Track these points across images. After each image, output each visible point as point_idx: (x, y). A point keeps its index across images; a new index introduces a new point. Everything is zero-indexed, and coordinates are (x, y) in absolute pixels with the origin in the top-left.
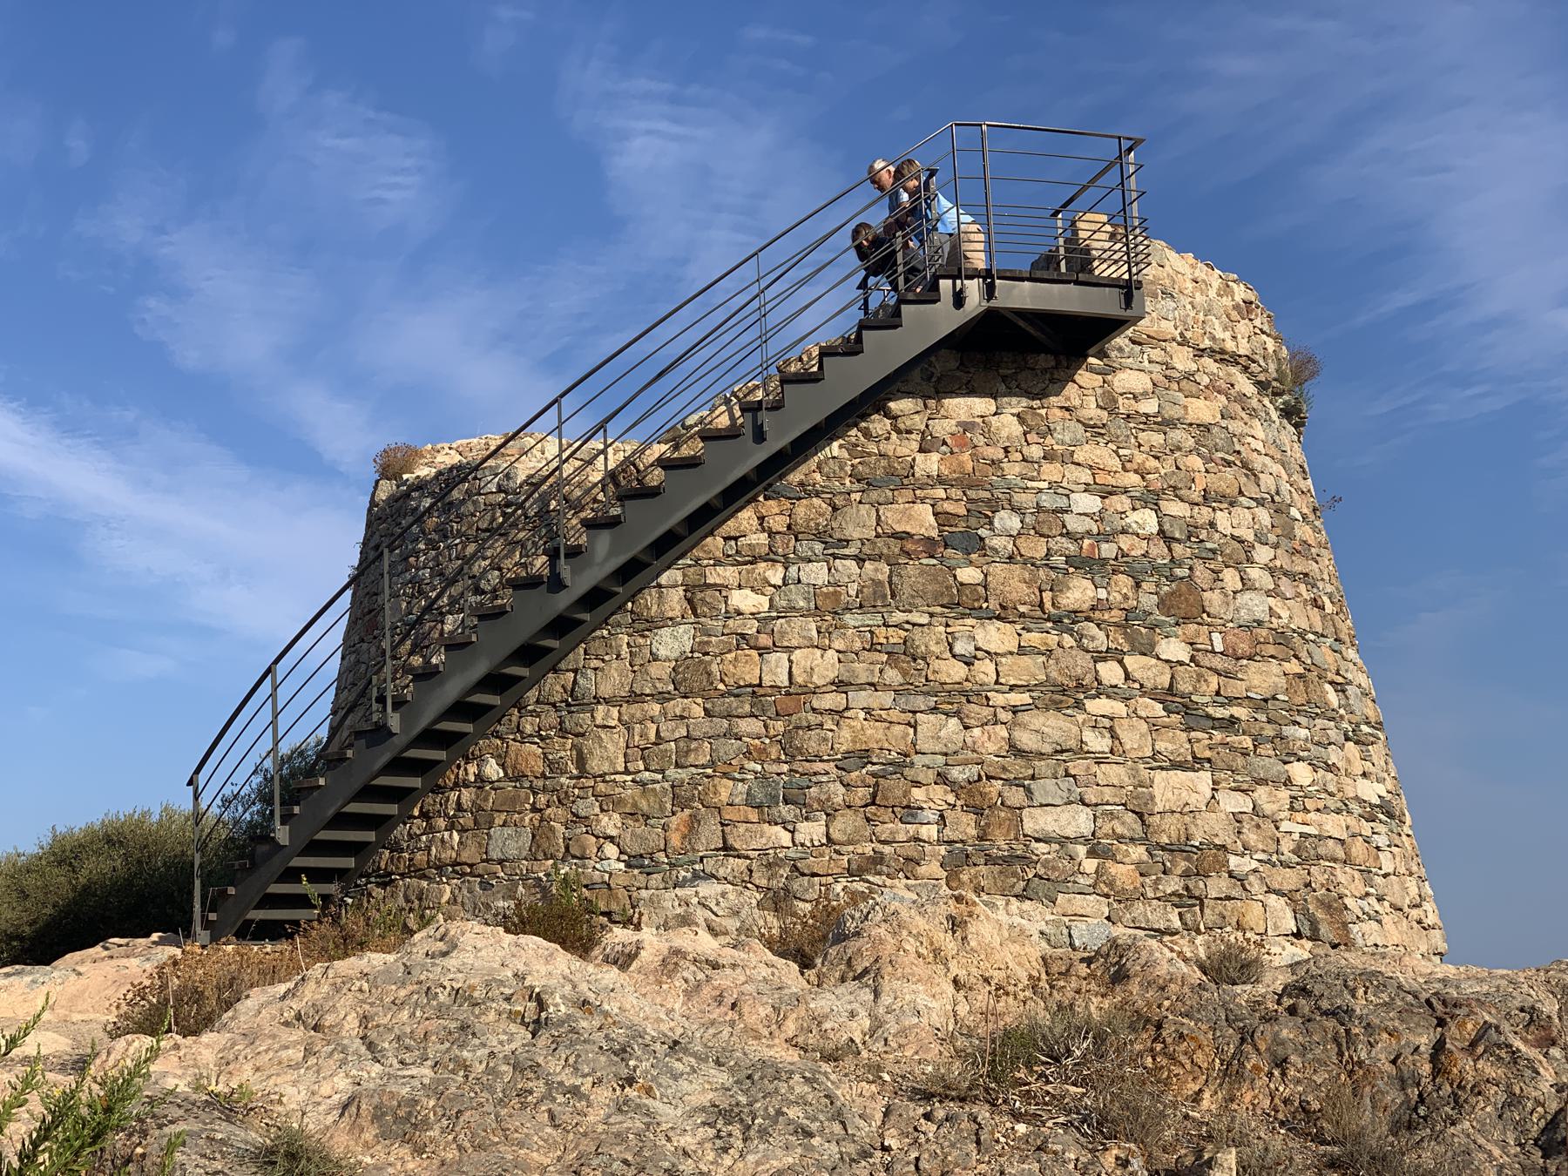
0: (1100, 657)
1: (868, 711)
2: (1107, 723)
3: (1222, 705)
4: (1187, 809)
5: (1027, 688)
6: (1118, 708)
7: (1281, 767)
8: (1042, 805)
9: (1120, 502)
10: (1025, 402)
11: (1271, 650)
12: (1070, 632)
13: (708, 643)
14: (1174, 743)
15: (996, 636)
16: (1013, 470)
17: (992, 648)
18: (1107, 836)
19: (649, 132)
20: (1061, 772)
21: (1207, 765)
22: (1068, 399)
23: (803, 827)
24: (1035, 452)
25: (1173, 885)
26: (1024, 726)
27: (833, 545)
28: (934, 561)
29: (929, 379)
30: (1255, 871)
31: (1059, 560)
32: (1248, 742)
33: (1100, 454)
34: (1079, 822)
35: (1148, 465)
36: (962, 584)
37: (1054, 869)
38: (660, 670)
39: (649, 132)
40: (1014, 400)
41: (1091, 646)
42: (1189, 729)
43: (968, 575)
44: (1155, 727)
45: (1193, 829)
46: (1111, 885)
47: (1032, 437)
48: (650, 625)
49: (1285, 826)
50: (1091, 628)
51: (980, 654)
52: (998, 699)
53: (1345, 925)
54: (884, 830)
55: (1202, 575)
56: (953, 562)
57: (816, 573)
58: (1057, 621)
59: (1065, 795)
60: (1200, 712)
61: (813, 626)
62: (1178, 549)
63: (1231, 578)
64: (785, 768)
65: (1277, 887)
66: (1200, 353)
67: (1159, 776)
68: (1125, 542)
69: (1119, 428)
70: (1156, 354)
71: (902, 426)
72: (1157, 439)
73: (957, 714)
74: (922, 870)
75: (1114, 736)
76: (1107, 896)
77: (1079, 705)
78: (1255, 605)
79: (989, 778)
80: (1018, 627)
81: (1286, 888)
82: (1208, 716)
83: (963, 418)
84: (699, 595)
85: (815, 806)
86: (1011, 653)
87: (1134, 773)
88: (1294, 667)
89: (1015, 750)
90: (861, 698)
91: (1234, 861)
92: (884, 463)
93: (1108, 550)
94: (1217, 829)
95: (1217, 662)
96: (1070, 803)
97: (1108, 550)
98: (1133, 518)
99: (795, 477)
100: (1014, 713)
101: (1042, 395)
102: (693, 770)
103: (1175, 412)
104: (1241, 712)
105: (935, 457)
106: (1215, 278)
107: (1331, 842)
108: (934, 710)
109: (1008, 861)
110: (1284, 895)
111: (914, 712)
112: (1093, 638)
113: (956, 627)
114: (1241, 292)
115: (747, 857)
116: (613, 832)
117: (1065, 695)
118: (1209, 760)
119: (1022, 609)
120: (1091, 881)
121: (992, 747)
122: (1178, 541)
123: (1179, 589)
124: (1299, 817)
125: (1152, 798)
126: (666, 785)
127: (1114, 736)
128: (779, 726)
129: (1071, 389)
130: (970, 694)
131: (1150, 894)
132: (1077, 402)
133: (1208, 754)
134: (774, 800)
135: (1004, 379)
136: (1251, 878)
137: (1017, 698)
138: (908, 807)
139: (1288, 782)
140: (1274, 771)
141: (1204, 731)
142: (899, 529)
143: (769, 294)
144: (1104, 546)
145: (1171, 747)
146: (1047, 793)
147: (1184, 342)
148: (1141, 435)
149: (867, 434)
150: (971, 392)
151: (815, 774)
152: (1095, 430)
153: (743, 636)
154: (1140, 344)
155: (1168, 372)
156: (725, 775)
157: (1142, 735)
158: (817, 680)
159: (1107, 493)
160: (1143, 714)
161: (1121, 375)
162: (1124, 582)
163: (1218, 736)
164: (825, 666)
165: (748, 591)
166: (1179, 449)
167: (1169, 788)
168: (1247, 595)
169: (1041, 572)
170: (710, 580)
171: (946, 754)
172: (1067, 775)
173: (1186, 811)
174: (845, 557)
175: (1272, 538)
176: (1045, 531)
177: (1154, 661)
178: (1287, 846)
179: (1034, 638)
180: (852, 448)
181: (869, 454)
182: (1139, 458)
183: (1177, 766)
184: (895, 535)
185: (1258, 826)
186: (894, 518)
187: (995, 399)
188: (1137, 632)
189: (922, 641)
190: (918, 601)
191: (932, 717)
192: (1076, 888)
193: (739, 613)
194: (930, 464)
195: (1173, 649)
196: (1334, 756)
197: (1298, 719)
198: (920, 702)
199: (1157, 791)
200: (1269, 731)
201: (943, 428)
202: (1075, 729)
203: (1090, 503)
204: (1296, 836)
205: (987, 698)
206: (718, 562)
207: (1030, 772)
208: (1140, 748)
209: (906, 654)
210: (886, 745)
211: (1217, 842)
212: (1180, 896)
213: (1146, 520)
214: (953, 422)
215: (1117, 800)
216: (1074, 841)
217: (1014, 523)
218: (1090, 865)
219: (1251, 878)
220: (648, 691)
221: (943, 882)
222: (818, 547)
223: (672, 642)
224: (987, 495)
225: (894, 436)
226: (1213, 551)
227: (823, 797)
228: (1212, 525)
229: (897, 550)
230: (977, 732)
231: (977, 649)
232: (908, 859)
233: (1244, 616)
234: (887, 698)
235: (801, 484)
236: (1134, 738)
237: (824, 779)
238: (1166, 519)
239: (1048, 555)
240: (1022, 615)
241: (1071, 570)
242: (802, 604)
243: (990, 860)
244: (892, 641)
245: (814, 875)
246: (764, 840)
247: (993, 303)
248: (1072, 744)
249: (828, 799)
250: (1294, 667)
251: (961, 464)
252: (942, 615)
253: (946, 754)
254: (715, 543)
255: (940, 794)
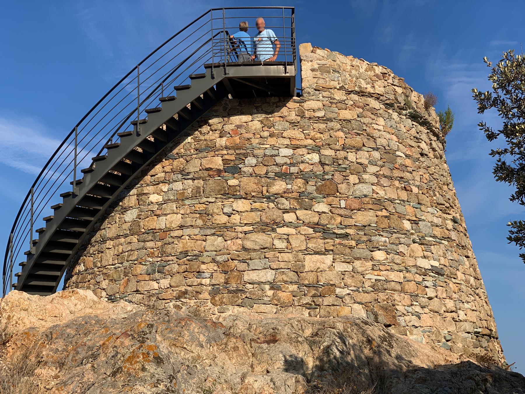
0: (286, 211)
1: (189, 236)
2: (286, 237)
3: (342, 229)
4: (319, 270)
5: (252, 224)
6: (292, 231)
7: (369, 253)
8: (253, 270)
9: (300, 151)
10: (264, 116)
11: (370, 206)
12: (273, 202)
13: (141, 215)
14: (318, 244)
15: (241, 205)
16: (255, 142)
17: (239, 210)
18: (280, 281)
19: (459, 82)
20: (263, 256)
21: (331, 252)
22: (282, 113)
23: (162, 281)
24: (266, 134)
25: (307, 300)
26: (248, 239)
27: (184, 174)
28: (220, 178)
29: (225, 110)
30: (349, 294)
31: (271, 175)
32: (353, 243)
33: (296, 133)
34: (269, 275)
35: (316, 136)
36: (230, 186)
37: (254, 294)
38: (126, 226)
39: (459, 82)
40: (259, 115)
41: (282, 207)
42: (325, 238)
43: (233, 182)
44: (308, 238)
45: (320, 278)
46: (279, 300)
47: (266, 128)
48: (125, 210)
49: (367, 277)
50: (284, 200)
51: (234, 212)
52: (239, 229)
53: (394, 317)
54: (189, 281)
55: (338, 177)
56: (227, 178)
57: (178, 186)
58: (268, 198)
59: (263, 265)
60: (331, 232)
61: (175, 206)
62: (327, 168)
63: (353, 179)
64: (159, 259)
65: (359, 300)
66: (349, 93)
67: (308, 257)
68: (302, 166)
69: (305, 122)
70: (326, 94)
71: (213, 129)
72: (322, 126)
73: (222, 236)
74: (201, 296)
75: (288, 242)
76: (277, 305)
77: (274, 230)
78: (365, 189)
79: (232, 260)
80: (251, 201)
81: (364, 301)
82: (334, 233)
83: (238, 124)
84: (141, 197)
85: (167, 273)
86: (247, 211)
87: (296, 256)
88: (384, 213)
89: (245, 249)
90: (187, 231)
91: (338, 290)
92: (205, 143)
93: (294, 170)
94: (332, 277)
95: (342, 212)
96: (266, 269)
97: (294, 170)
98: (307, 157)
99: (175, 151)
100: (245, 234)
101: (272, 112)
102: (130, 262)
103: (332, 115)
104: (351, 231)
105: (224, 139)
106: (365, 65)
107: (393, 283)
108: (214, 234)
109: (237, 291)
110: (362, 304)
111: (206, 236)
112: (283, 204)
113: (226, 202)
114: (379, 70)
115: (143, 294)
116: (105, 287)
117: (268, 226)
118: (332, 250)
119: (253, 194)
120: (269, 299)
121: (234, 248)
122: (328, 165)
123: (326, 183)
124: (376, 273)
125: (304, 266)
126: (122, 268)
127: (288, 242)
128: (159, 244)
129: (284, 110)
130: (230, 228)
131: (296, 304)
132: (286, 114)
133: (332, 248)
134: (154, 271)
135: (257, 108)
136: (346, 297)
137: (246, 228)
138: (198, 272)
139: (372, 259)
140: (365, 254)
141: (332, 239)
142: (207, 167)
143: (164, 84)
144: (292, 168)
145: (314, 245)
146: (255, 265)
147: (341, 88)
148: (315, 125)
149: (201, 133)
150: (242, 113)
151: (169, 261)
152: (294, 124)
153: (152, 211)
154: (319, 91)
155: (331, 101)
156: (140, 263)
157: (301, 241)
158: (173, 225)
159: (296, 148)
160: (303, 233)
161: (308, 103)
162: (300, 182)
163: (338, 241)
164: (176, 220)
165: (156, 195)
166: (332, 129)
167: (311, 262)
168: (360, 186)
169: (263, 179)
170: (145, 192)
171: (216, 251)
172: (265, 258)
173: (318, 271)
174: (188, 179)
175: (380, 163)
176: (266, 164)
177: (313, 212)
178: (367, 284)
179: (257, 205)
180: (196, 140)
181: (201, 140)
182: (312, 133)
183: (317, 253)
184: (207, 169)
185: (353, 276)
186: (206, 163)
187: (252, 115)
188: (303, 200)
189: (212, 208)
190: (212, 193)
191: (212, 237)
192: (262, 302)
193: (152, 203)
194: (223, 142)
195: (322, 207)
196: (402, 248)
197: (382, 233)
198: (209, 232)
199: (306, 263)
200: (365, 238)
201: (228, 128)
202: (270, 240)
203: (289, 152)
204: (373, 281)
205: (235, 229)
206: (148, 185)
207: (249, 257)
208: (299, 246)
209: (205, 214)
210: (194, 249)
211: (331, 283)
212: (310, 304)
213: (315, 157)
214: (234, 125)
215: (286, 267)
216: (265, 283)
217: (254, 161)
218: (270, 293)
219: (346, 297)
220: (121, 234)
221: (209, 301)
222: (180, 176)
223: (130, 216)
224: (244, 151)
225: (211, 132)
226: (346, 168)
227: (170, 270)
228: (346, 158)
229: (206, 175)
230: (229, 242)
231: (234, 210)
232: (197, 292)
233: (358, 193)
234: (196, 231)
235: (177, 154)
236: (297, 242)
237: (171, 262)
238: (323, 156)
239: (267, 173)
240: (253, 196)
241: (276, 178)
242: (172, 198)
243: (230, 292)
244: (201, 209)
245: (164, 299)
246: (149, 287)
247: (227, 76)
248: (268, 245)
249: (171, 270)
250: (384, 213)
251: (234, 141)
252: (220, 198)
253: (216, 251)
254: (148, 178)
255: (213, 267)
